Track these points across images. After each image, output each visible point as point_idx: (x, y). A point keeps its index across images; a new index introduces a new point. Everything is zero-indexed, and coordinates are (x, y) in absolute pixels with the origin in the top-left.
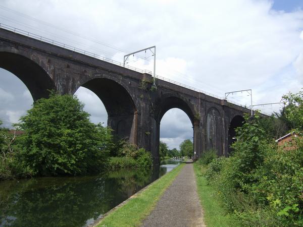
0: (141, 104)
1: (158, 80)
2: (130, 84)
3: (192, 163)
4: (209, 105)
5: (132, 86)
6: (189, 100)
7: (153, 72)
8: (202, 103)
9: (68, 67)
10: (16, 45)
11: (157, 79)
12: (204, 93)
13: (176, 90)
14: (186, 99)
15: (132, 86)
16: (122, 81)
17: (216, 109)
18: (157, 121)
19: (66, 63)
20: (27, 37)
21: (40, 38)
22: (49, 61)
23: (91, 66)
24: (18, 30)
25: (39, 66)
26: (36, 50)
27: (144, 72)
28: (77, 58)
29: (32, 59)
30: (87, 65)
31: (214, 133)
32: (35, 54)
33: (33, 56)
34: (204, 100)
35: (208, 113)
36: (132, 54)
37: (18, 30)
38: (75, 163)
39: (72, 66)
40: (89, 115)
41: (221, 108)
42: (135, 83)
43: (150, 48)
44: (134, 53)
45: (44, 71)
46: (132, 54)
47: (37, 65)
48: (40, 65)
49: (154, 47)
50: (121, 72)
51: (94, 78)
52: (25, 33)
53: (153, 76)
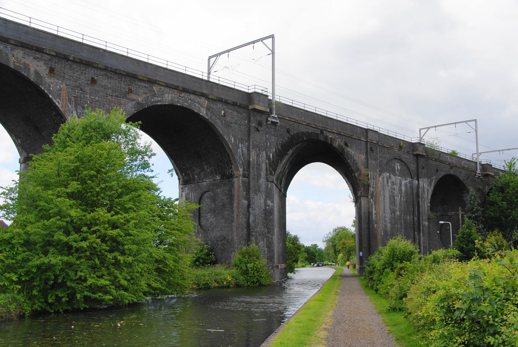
1: (278, 104)
2: (225, 115)
3: (356, 276)
5: (228, 119)
7: (270, 90)
11: (280, 103)
12: (376, 129)
14: (338, 143)
15: (228, 119)
16: (208, 109)
17: (401, 160)
18: (280, 191)
19: (91, 73)
20: (355, 126)
21: (346, 119)
22: (52, 71)
23: (141, 80)
24: (319, 110)
25: (29, 81)
26: (23, 45)
29: (12, 66)
30: (133, 77)
31: (398, 213)
32: (19, 53)
36: (433, 127)
37: (319, 110)
39: (103, 80)
40: (353, 201)
42: (235, 114)
43: (262, 40)
44: (228, 51)
45: (43, 91)
46: (433, 127)
47: (26, 81)
48: (32, 78)
49: (272, 37)
50: (205, 92)
53: (270, 98)
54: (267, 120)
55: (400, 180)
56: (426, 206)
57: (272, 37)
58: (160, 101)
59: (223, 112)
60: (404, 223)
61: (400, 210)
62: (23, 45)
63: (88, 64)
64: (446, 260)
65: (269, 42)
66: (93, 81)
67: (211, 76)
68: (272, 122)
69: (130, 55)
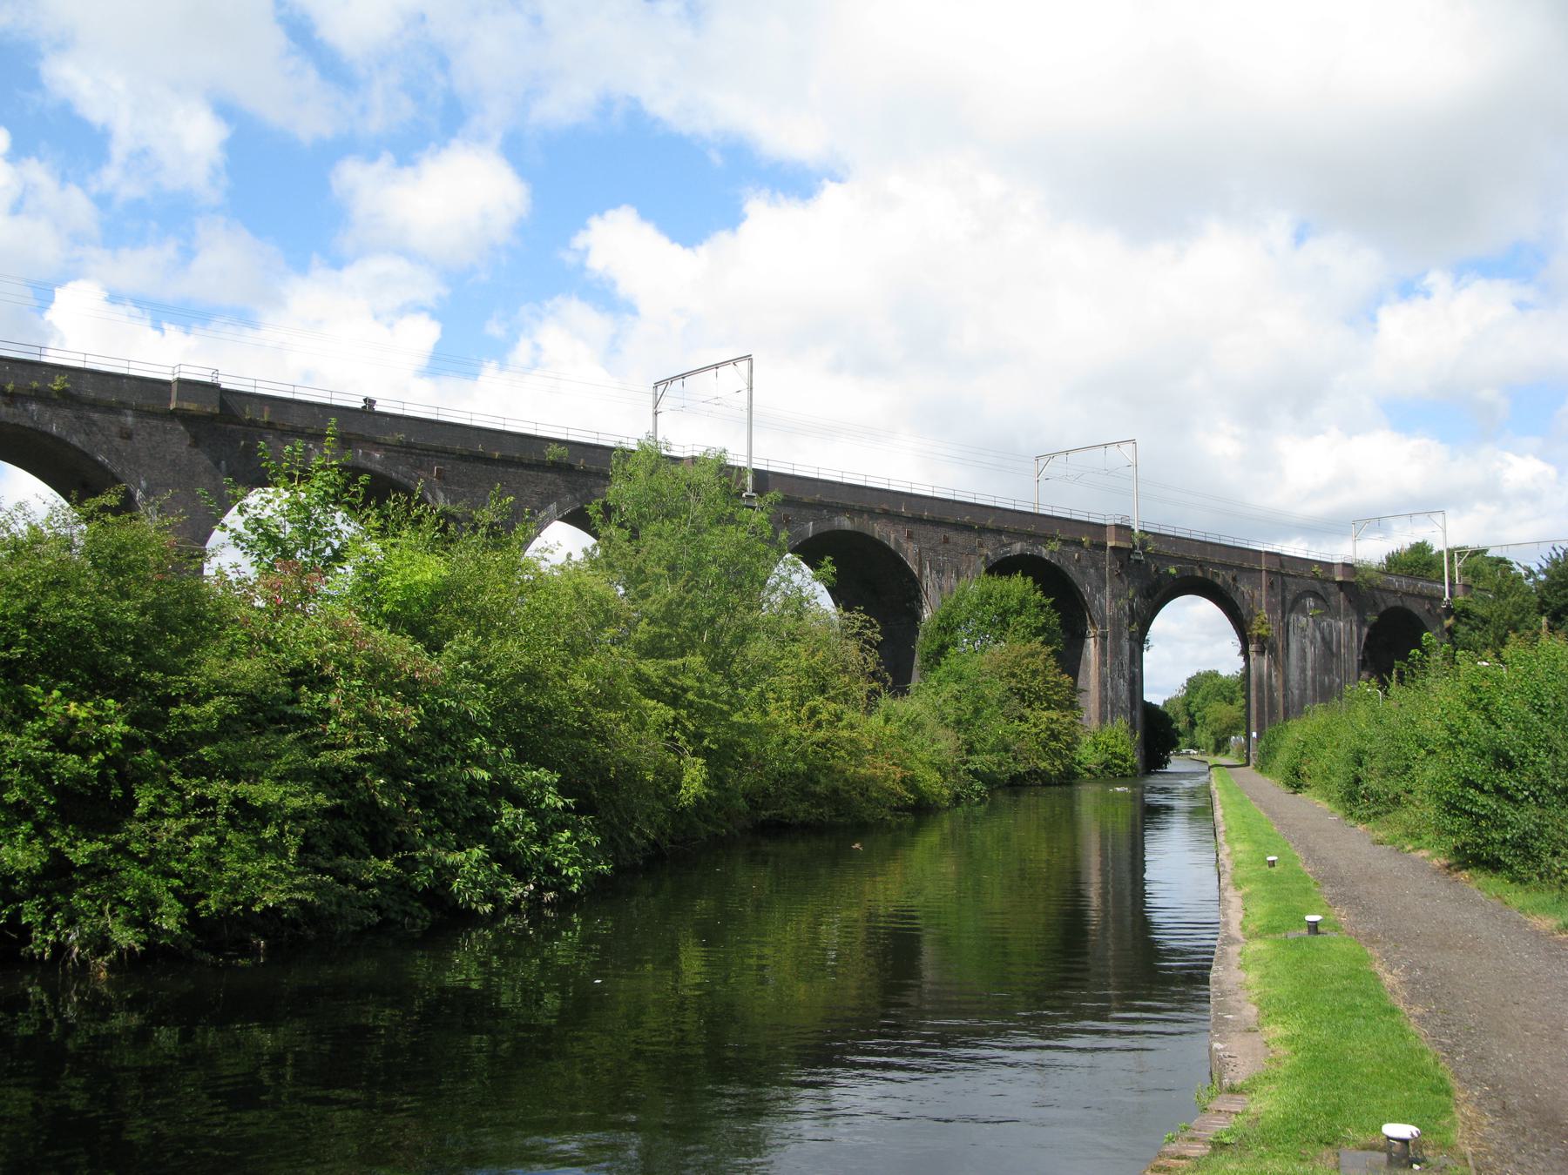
0: (1106, 601)
2: (1079, 560)
4: (1294, 587)
6: (1234, 579)
8: (1272, 583)
9: (946, 541)
10: (1018, 535)
13: (1197, 556)
14: (1222, 578)
17: (1315, 595)
19: (942, 533)
22: (910, 537)
24: (413, 407)
26: (886, 514)
27: (1340, 561)
28: (552, 453)
29: (877, 537)
33: (879, 530)
34: (1276, 573)
35: (1291, 610)
37: (799, 468)
38: (503, 801)
41: (1333, 588)
44: (717, 366)
47: (887, 549)
48: (892, 546)
49: (749, 358)
51: (999, 557)
52: (902, 484)
54: (1129, 559)
55: (306, 449)
56: (1355, 660)
57: (749, 358)
58: (1009, 552)
59: (1076, 555)
60: (1320, 687)
61: (1314, 669)
62: (886, 514)
63: (937, 523)
64: (1218, 698)
65: (744, 365)
66: (946, 541)
67: (754, 460)
68: (1136, 560)
69: (797, 473)
